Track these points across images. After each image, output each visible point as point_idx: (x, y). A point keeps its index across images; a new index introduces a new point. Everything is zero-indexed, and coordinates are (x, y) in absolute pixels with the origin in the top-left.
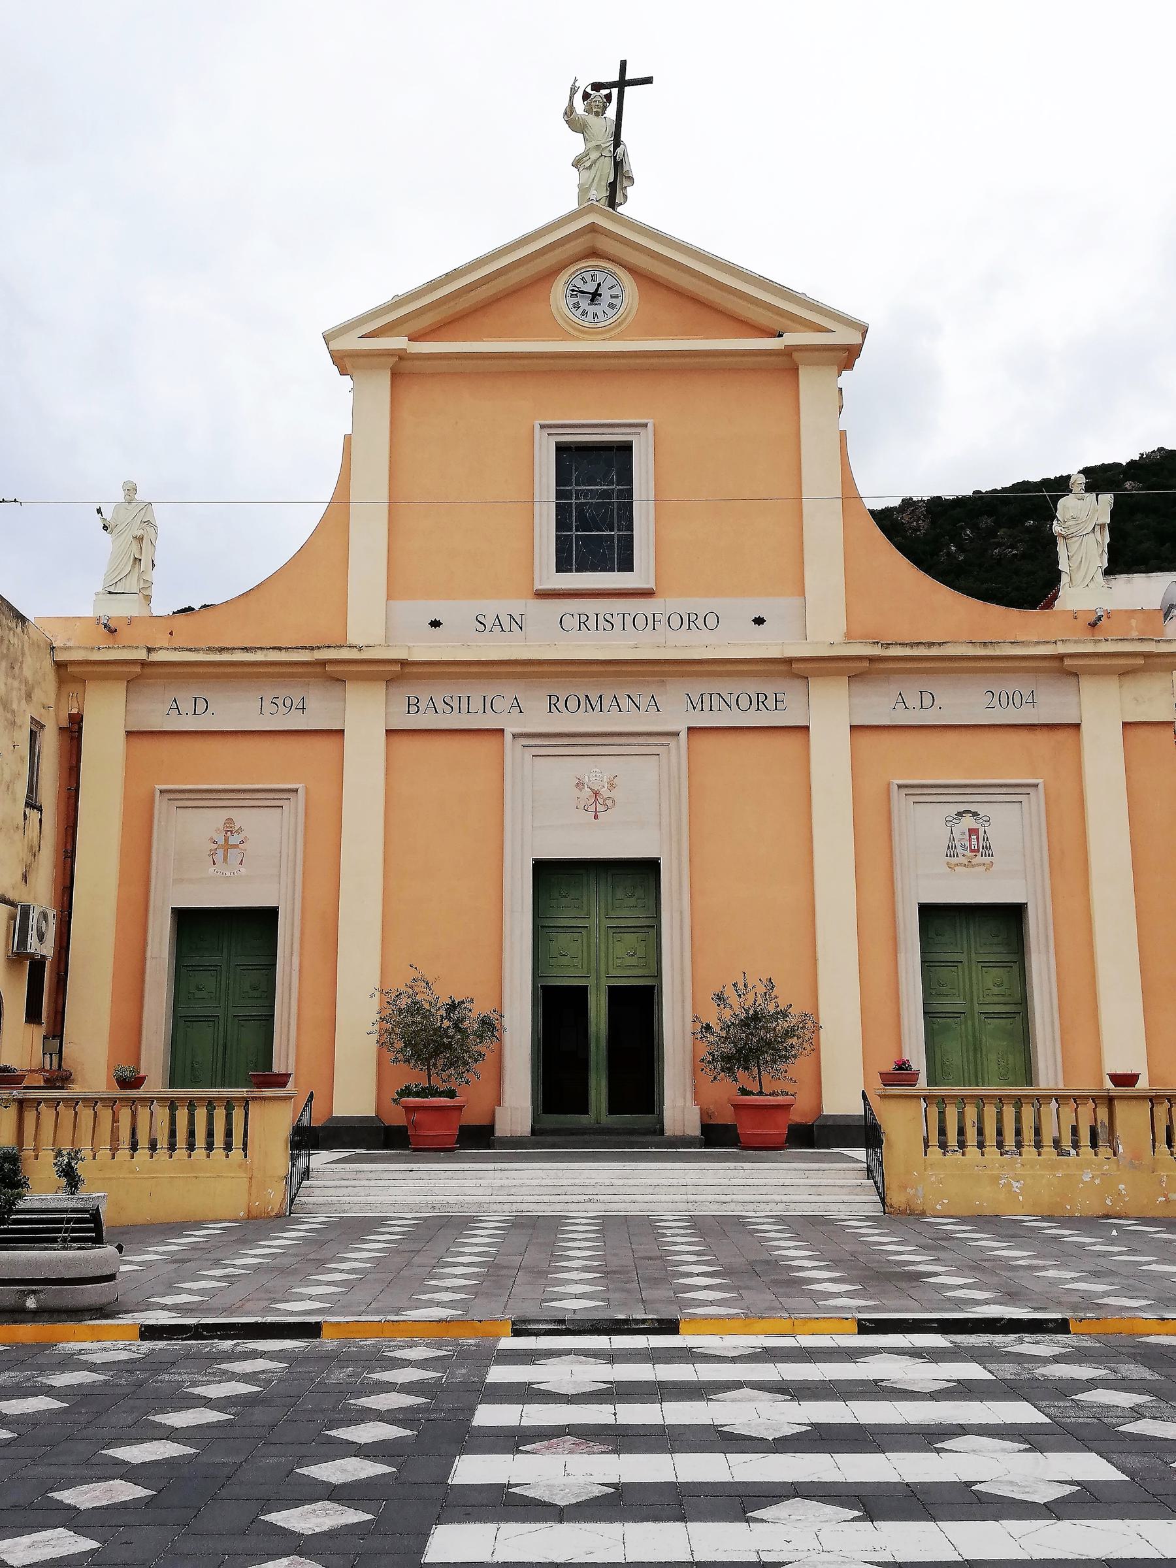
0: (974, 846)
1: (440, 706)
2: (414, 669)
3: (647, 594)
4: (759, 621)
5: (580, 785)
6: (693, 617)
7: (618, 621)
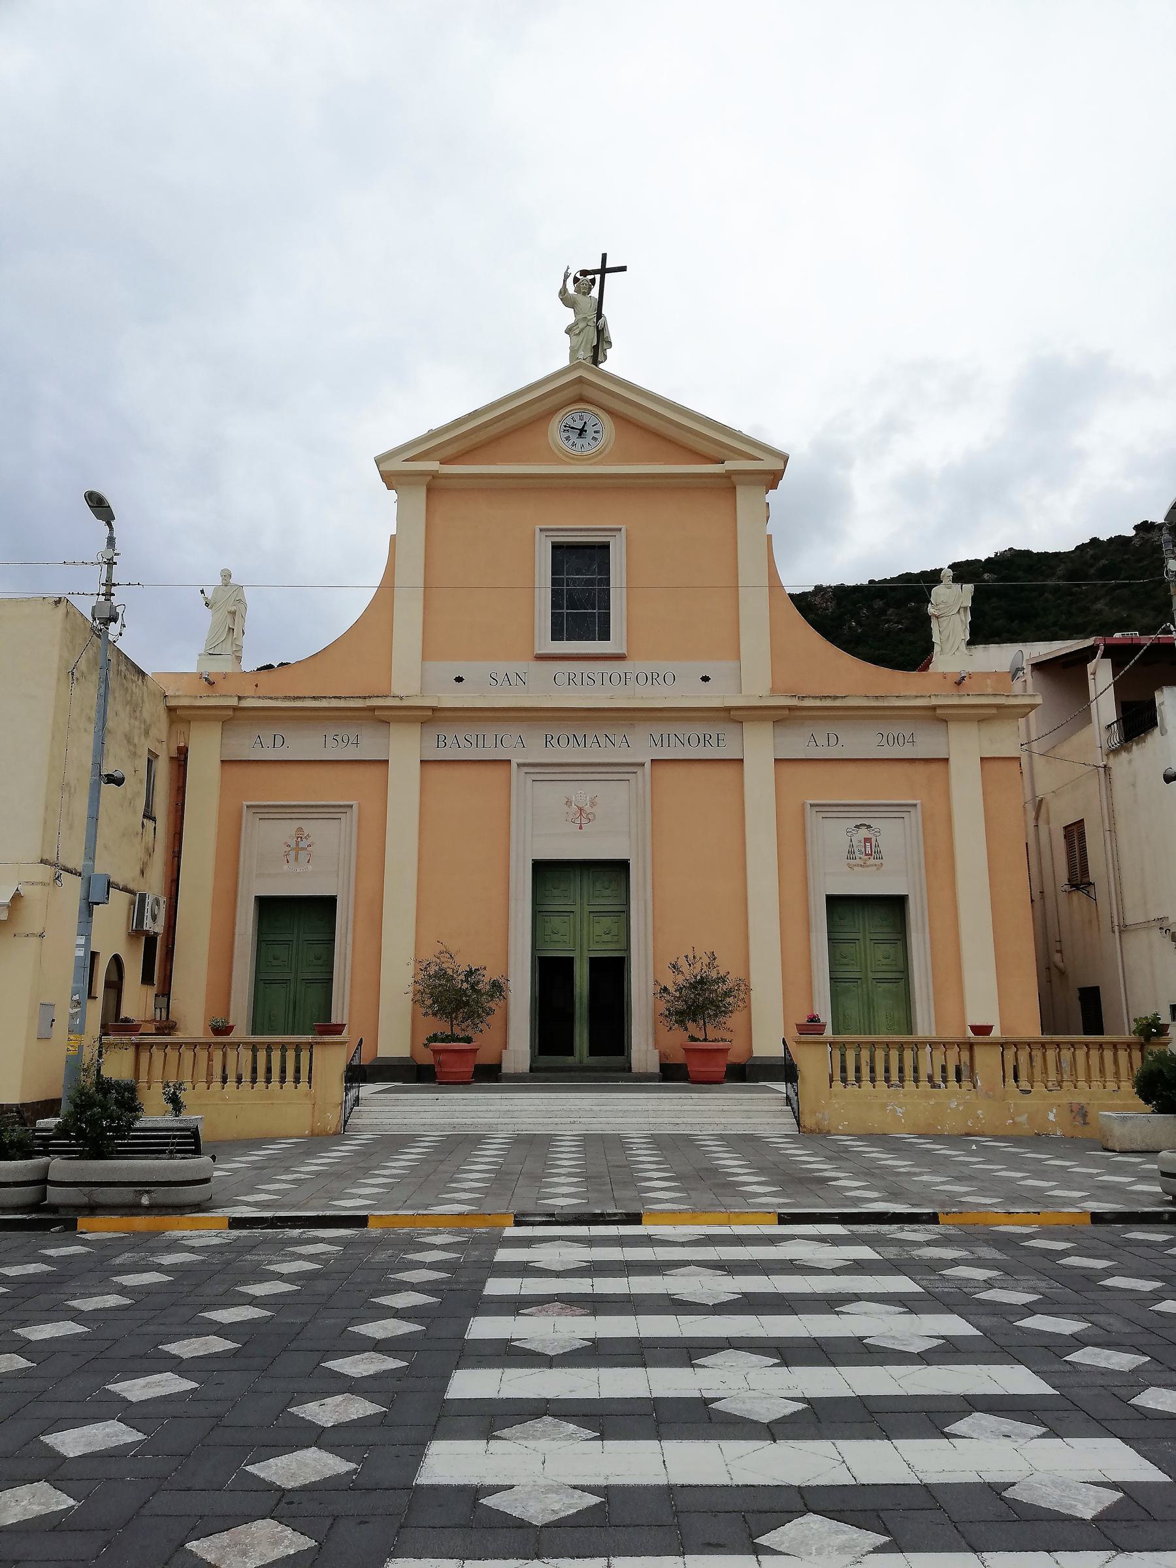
3: (620, 657)
4: (705, 679)
6: (655, 676)
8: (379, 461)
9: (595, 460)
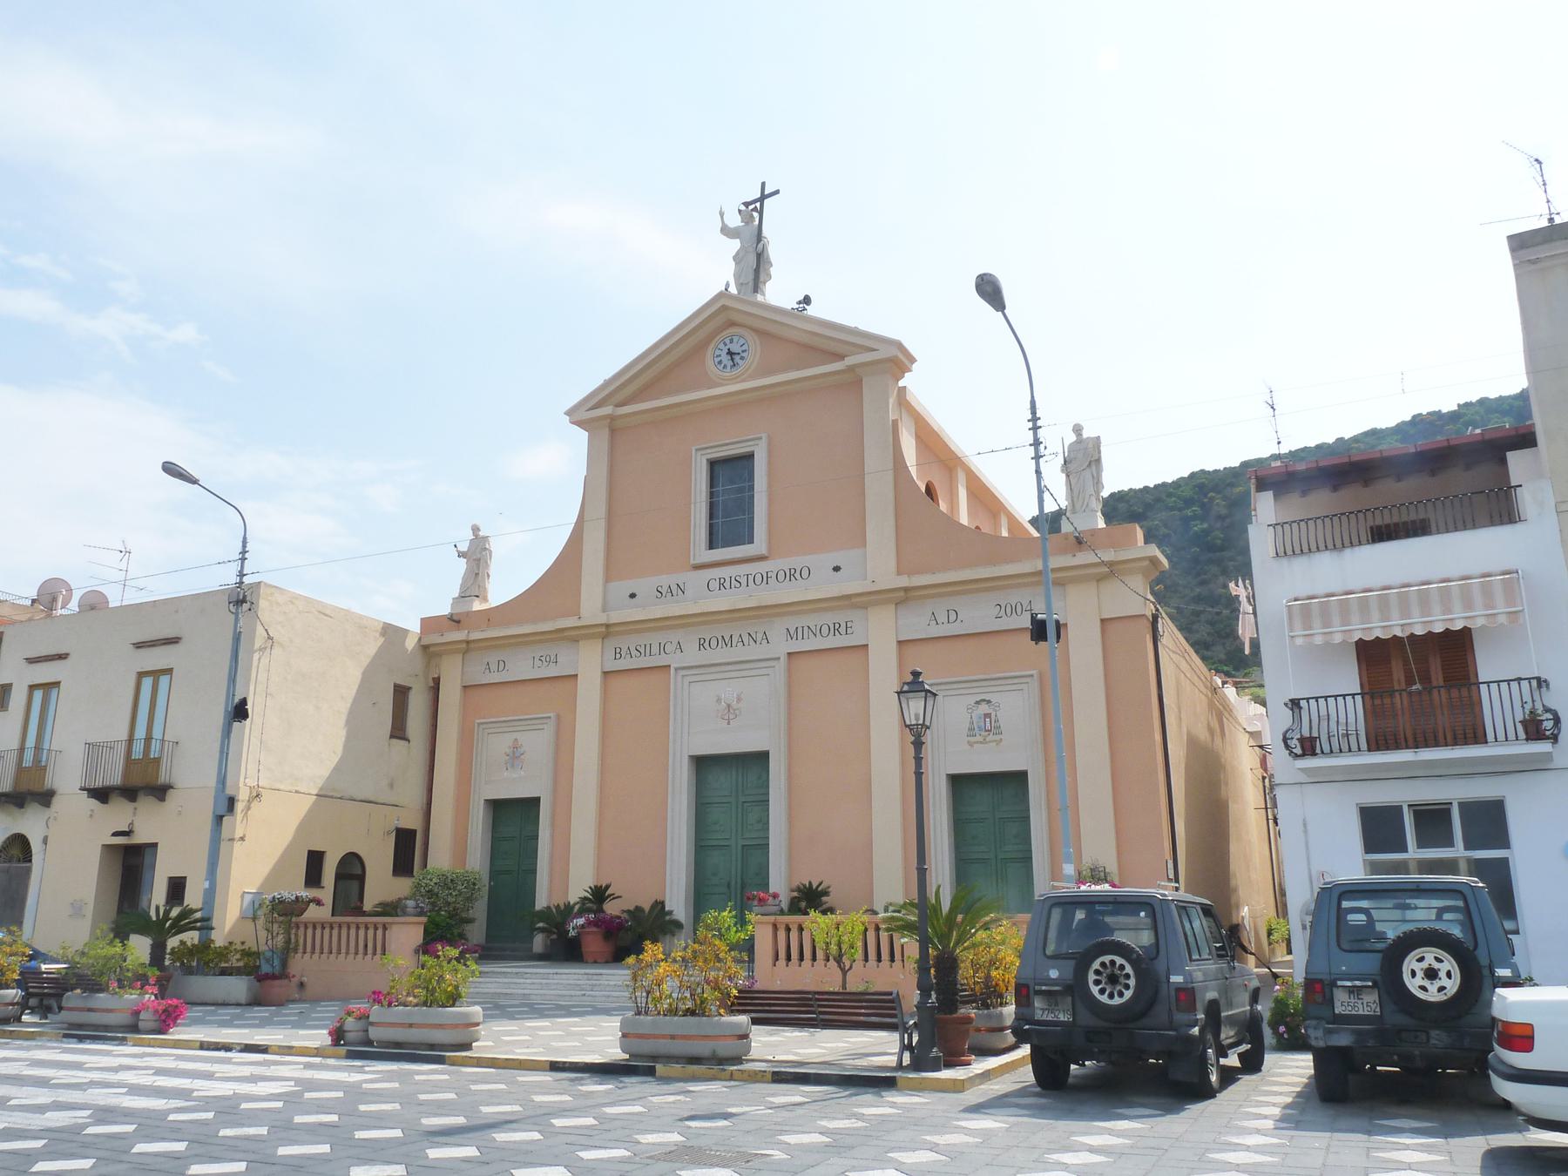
0: (989, 728)
1: (634, 653)
2: (617, 629)
3: (762, 558)
4: (837, 569)
5: (719, 700)
6: (793, 571)
7: (744, 581)
8: (568, 413)
9: (738, 380)
